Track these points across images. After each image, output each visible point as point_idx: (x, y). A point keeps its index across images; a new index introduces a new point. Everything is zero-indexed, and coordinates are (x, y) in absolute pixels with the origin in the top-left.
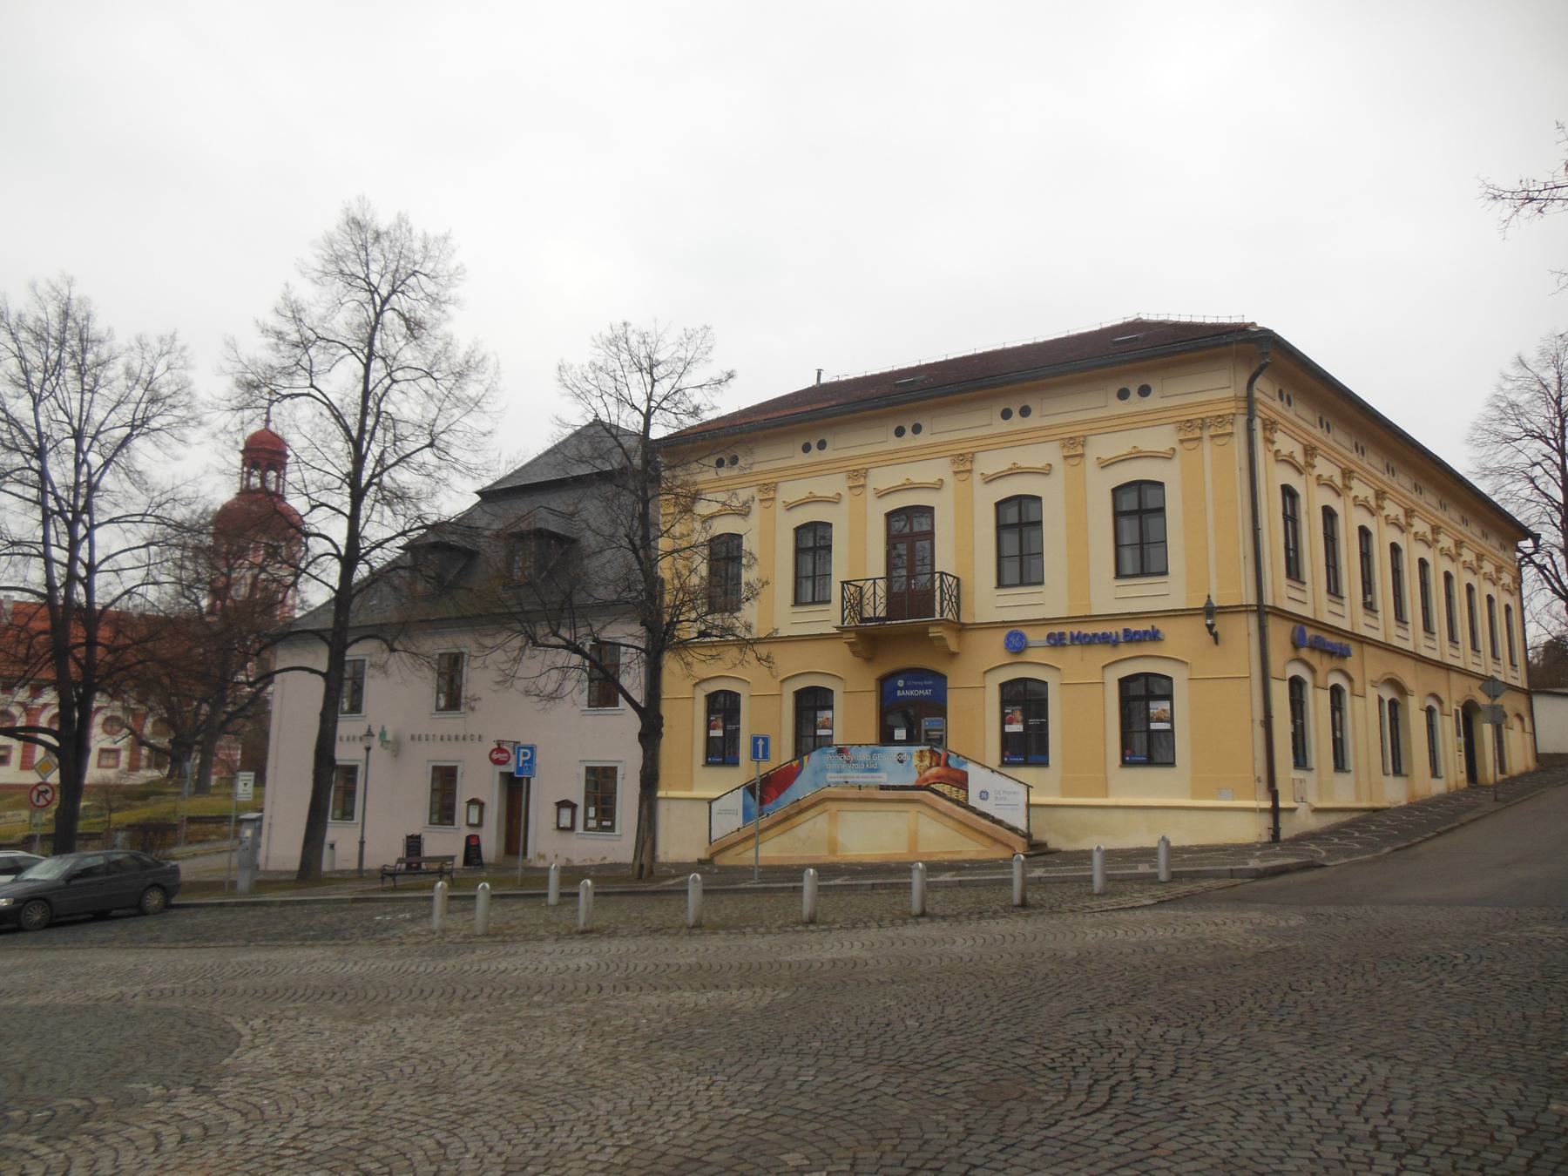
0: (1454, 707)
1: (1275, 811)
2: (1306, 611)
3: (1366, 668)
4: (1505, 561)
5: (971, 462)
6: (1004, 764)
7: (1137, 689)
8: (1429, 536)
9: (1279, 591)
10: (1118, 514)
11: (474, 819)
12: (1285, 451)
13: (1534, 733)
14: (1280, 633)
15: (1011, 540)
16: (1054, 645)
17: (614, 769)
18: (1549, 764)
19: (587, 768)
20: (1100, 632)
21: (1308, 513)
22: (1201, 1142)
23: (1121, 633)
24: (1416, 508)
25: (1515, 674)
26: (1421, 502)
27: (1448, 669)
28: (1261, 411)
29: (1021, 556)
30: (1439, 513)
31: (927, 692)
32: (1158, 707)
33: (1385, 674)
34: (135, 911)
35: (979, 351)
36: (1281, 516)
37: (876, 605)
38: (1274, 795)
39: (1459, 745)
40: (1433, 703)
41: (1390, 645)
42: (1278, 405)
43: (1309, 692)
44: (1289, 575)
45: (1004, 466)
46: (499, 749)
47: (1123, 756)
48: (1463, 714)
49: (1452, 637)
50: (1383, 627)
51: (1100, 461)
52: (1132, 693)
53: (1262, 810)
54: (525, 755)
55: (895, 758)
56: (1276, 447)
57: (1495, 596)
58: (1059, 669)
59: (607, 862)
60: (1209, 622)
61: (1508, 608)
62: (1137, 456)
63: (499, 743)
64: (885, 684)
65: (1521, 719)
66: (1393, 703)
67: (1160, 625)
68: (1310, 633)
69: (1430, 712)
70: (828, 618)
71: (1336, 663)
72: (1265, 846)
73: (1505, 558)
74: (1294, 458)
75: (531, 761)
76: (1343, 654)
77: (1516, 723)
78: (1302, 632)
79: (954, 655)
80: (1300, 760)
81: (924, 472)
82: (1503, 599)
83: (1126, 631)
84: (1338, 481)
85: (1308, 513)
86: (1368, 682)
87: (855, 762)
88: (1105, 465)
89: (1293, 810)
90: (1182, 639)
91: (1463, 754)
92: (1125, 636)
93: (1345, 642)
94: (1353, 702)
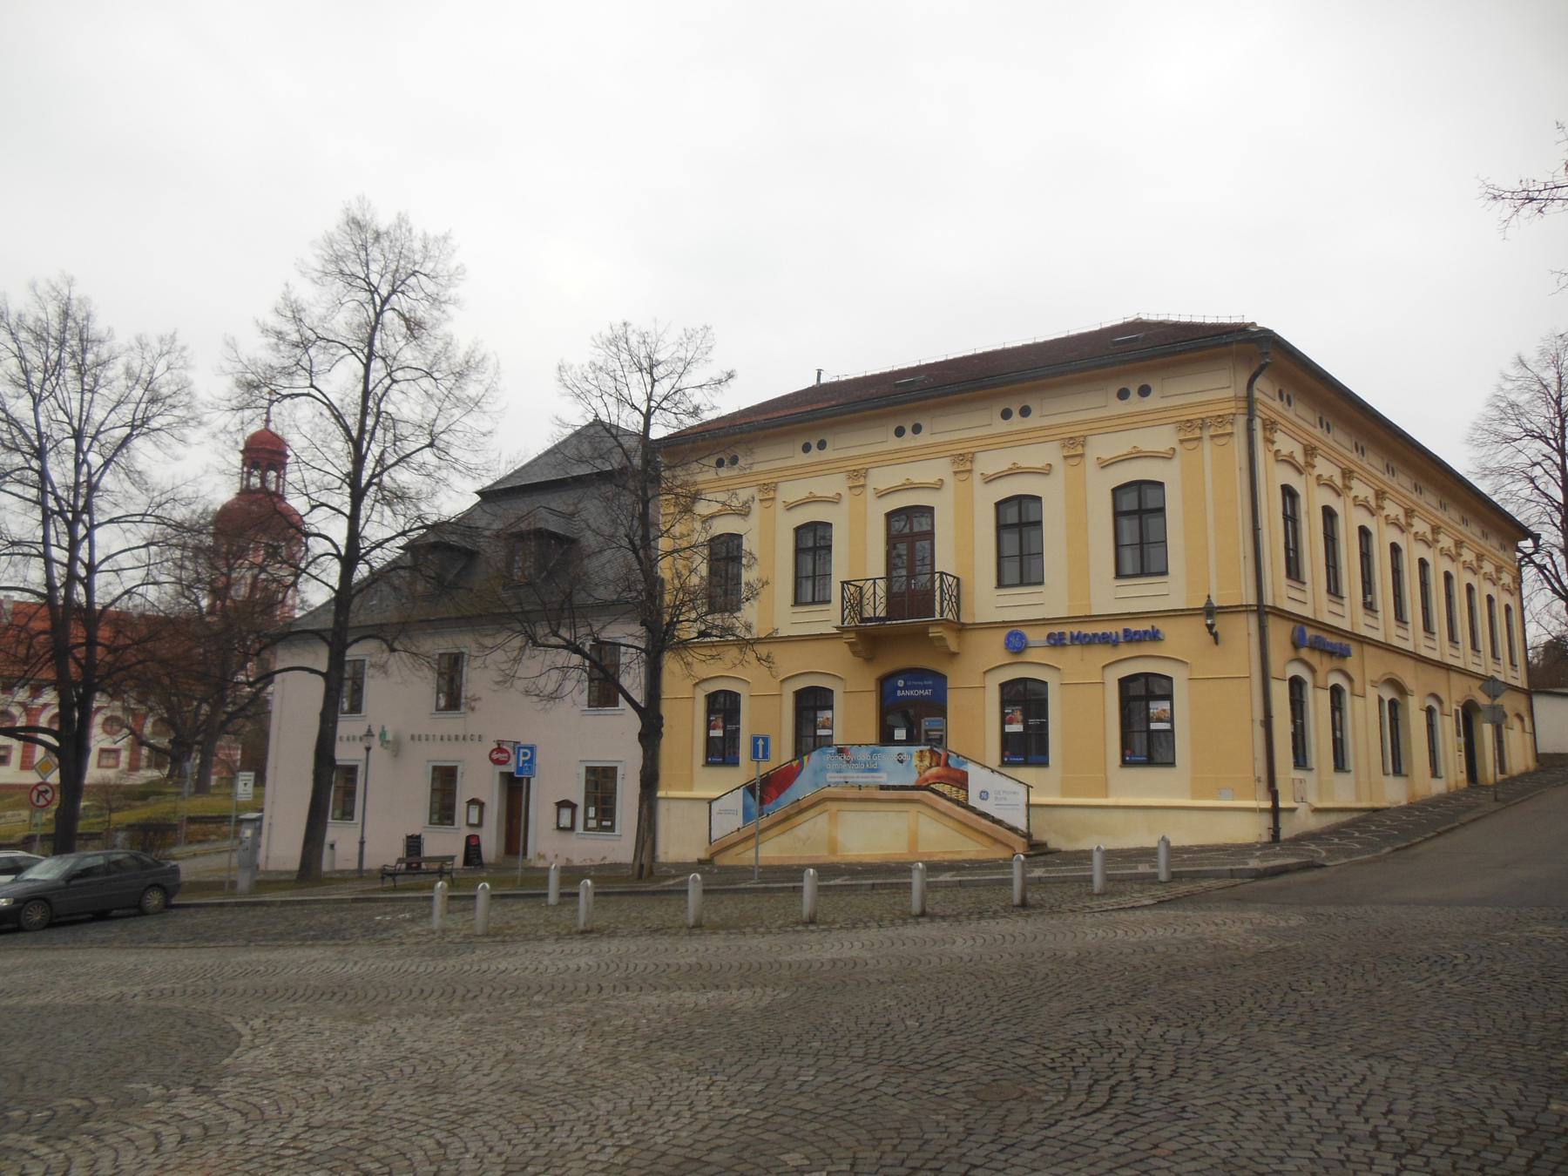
0: (1454, 707)
1: (1275, 811)
2: (1306, 611)
3: (1366, 668)
4: (1505, 561)
5: (971, 462)
6: (1004, 764)
7: (1137, 689)
8: (1429, 536)
9: (1279, 591)
10: (1118, 514)
11: (474, 819)
12: (1285, 451)
13: (1534, 733)
14: (1280, 633)
15: (1011, 540)
16: (1054, 645)
17: (614, 769)
18: (1549, 764)
19: (587, 768)
20: (1100, 632)
21: (1308, 513)
22: (1201, 1142)
23: (1121, 633)
24: (1416, 508)
25: (1515, 674)
26: (1421, 502)
27: (1448, 669)
28: (1261, 411)
29: (1021, 556)
30: (1439, 513)
31: (927, 692)
32: (1158, 707)
33: (1385, 674)
34: (135, 911)
35: (979, 351)
36: (1281, 516)
37: (876, 605)
38: (1274, 795)
39: (1459, 745)
40: (1433, 703)
41: (1390, 645)
42: (1278, 405)
43: (1309, 692)
44: (1289, 575)
45: (1004, 466)
46: (499, 749)
47: (1123, 756)
48: (1463, 714)
49: (1452, 637)
50: (1383, 627)
51: (1100, 461)
52: (1132, 693)
53: (1262, 810)
54: (525, 755)
55: (895, 758)
56: (1276, 447)
57: (1495, 596)
58: (1059, 669)
59: (607, 862)
60: (1209, 622)
61: (1508, 608)
62: (1137, 456)
63: (499, 743)
64: (885, 684)
65: (1521, 719)
66: (1393, 703)
67: (1160, 625)
68: (1310, 633)
69: (1430, 712)
70: (828, 618)
71: (1336, 663)
72: (1265, 846)
73: (1505, 558)
74: (1294, 458)
75: (531, 761)
76: (1343, 654)
77: (1516, 723)
78: (1302, 632)
79: (954, 655)
80: (1300, 760)
81: (924, 472)
82: (1503, 599)
83: (1126, 631)
84: (1338, 481)
85: (1308, 513)
86: (1368, 682)
87: (855, 762)
88: (1105, 465)
89: (1293, 810)
90: (1182, 639)
91: (1463, 754)
92: (1125, 636)
93: (1345, 642)
94: (1353, 702)
